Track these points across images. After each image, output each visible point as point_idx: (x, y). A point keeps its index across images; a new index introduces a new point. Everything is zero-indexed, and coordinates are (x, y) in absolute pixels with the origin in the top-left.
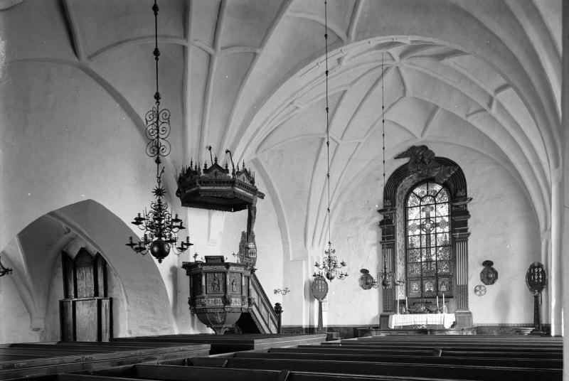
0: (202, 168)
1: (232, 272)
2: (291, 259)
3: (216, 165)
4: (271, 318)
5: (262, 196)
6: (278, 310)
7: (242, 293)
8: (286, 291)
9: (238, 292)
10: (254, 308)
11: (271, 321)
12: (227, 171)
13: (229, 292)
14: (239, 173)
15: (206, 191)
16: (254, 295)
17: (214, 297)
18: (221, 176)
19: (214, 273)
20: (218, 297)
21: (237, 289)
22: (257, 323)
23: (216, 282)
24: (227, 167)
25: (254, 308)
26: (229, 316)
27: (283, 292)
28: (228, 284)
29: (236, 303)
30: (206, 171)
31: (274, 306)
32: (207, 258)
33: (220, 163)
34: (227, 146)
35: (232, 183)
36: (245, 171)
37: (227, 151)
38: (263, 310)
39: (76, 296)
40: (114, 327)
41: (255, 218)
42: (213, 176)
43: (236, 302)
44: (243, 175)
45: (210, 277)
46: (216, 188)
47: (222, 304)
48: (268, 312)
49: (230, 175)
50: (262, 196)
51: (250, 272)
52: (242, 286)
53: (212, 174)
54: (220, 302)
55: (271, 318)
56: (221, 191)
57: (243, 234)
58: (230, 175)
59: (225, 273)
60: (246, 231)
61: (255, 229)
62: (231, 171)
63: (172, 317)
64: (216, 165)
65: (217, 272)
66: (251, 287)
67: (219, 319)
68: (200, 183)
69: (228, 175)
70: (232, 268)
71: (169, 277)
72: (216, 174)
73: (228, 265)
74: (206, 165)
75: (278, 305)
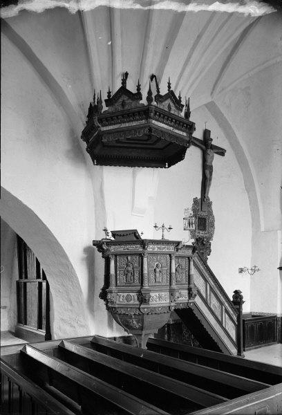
0: (105, 97)
1: (153, 254)
2: (263, 229)
3: (123, 90)
4: (227, 312)
5: (222, 152)
6: (238, 299)
7: (170, 284)
8: (254, 270)
9: (165, 281)
10: (198, 300)
11: (225, 316)
12: (138, 96)
13: (146, 286)
14: (160, 98)
15: (109, 132)
16: (198, 282)
17: (124, 291)
18: (131, 105)
19: (126, 255)
20: (132, 292)
21: (163, 279)
22: (204, 323)
23: (130, 269)
24: (139, 89)
25: (198, 300)
26: (147, 319)
27: (250, 271)
28: (145, 272)
29: (159, 299)
30: (109, 102)
31: (231, 295)
32: (114, 234)
33: (131, 86)
34: (150, 70)
35: (145, 112)
36: (171, 94)
37: (153, 77)
38: (214, 302)
39: (26, 277)
40: (51, 312)
41: (210, 180)
42: (120, 108)
43: (160, 297)
44: (168, 101)
45: (122, 261)
46: (123, 125)
47: (138, 303)
48: (221, 304)
49: (144, 101)
50: (222, 152)
51: (191, 251)
52: (170, 274)
53: (118, 106)
54: (134, 301)
55: (227, 312)
56: (129, 130)
57: (195, 201)
58: (144, 101)
59: (141, 256)
60: (199, 197)
61: (212, 194)
62: (145, 94)
63: (87, 312)
64: (123, 90)
65: (120, 255)
66: (193, 271)
67: (135, 323)
68: (100, 121)
69: (141, 102)
70: (150, 248)
71: (83, 260)
72: (123, 104)
73: (144, 243)
74: (109, 93)
75: (237, 293)
